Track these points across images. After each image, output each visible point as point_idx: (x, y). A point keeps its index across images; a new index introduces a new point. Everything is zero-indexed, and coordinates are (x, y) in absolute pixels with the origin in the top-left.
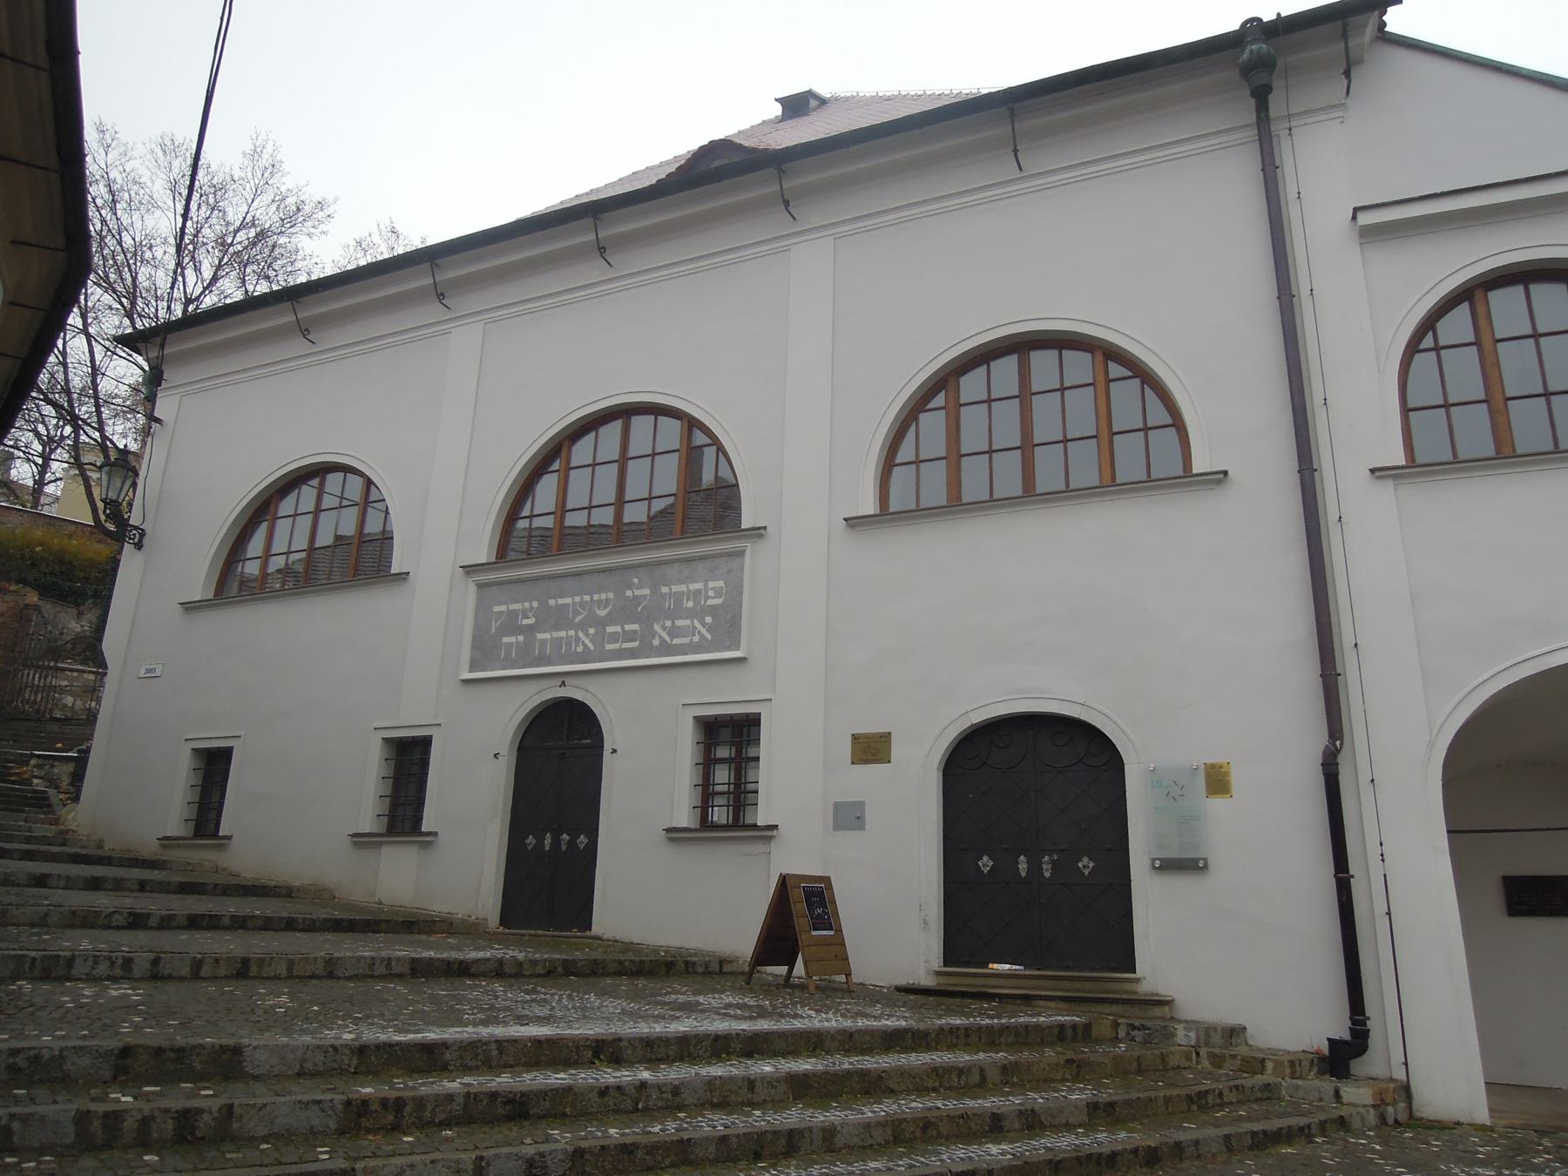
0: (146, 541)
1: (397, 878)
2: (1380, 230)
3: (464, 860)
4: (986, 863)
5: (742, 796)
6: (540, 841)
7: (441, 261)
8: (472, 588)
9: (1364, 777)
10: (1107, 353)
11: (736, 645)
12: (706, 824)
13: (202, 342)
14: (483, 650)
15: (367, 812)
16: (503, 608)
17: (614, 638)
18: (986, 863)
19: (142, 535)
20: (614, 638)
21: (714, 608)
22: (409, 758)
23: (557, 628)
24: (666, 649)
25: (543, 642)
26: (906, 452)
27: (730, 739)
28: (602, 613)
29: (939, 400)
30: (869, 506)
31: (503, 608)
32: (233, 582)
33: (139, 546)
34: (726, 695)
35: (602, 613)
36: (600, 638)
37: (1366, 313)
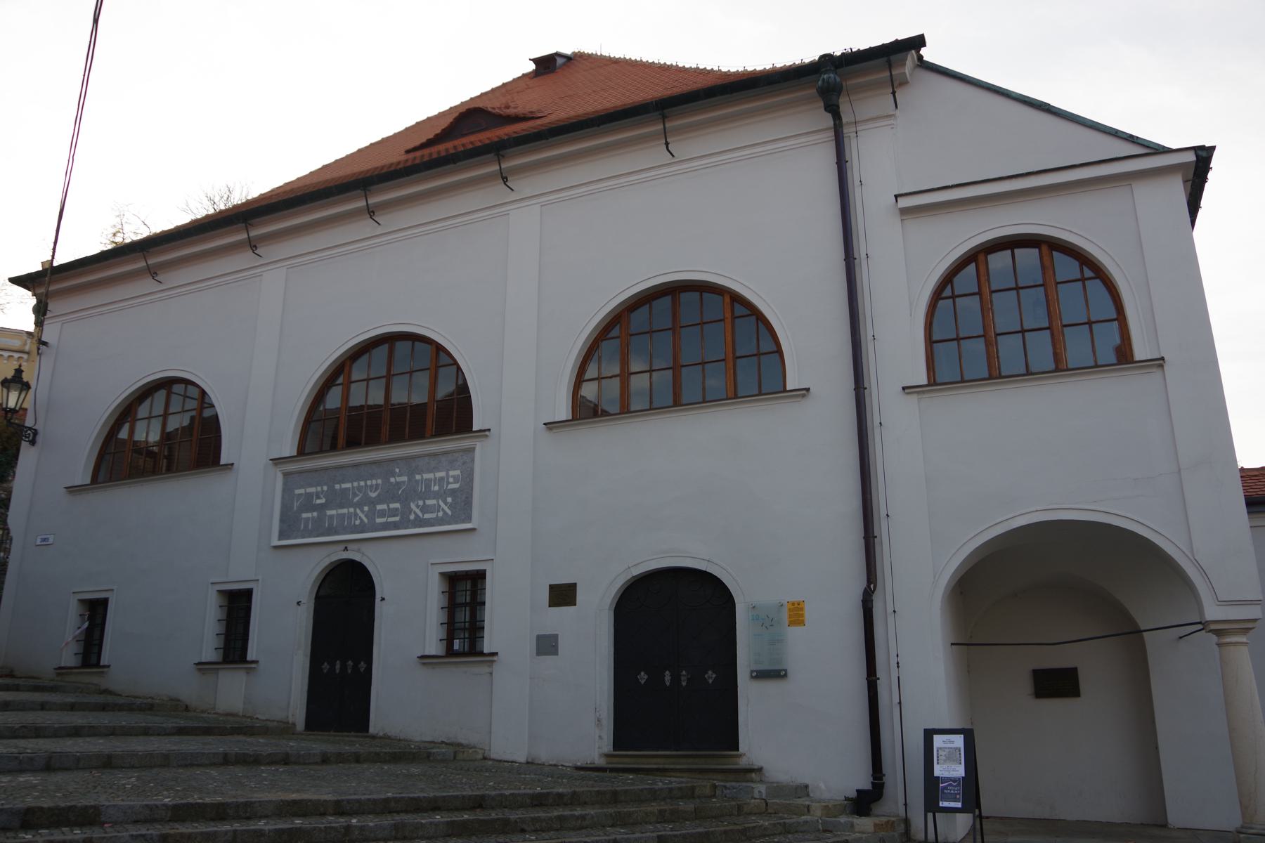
0: (39, 438)
2: (916, 209)
4: (643, 677)
5: (475, 629)
6: (333, 666)
8: (280, 478)
10: (736, 299)
11: (468, 519)
12: (450, 652)
17: (382, 514)
19: (36, 433)
20: (382, 514)
21: (453, 491)
24: (420, 522)
25: (331, 517)
27: (465, 592)
28: (373, 495)
33: (33, 442)
34: (462, 557)
35: (373, 495)
36: (372, 515)
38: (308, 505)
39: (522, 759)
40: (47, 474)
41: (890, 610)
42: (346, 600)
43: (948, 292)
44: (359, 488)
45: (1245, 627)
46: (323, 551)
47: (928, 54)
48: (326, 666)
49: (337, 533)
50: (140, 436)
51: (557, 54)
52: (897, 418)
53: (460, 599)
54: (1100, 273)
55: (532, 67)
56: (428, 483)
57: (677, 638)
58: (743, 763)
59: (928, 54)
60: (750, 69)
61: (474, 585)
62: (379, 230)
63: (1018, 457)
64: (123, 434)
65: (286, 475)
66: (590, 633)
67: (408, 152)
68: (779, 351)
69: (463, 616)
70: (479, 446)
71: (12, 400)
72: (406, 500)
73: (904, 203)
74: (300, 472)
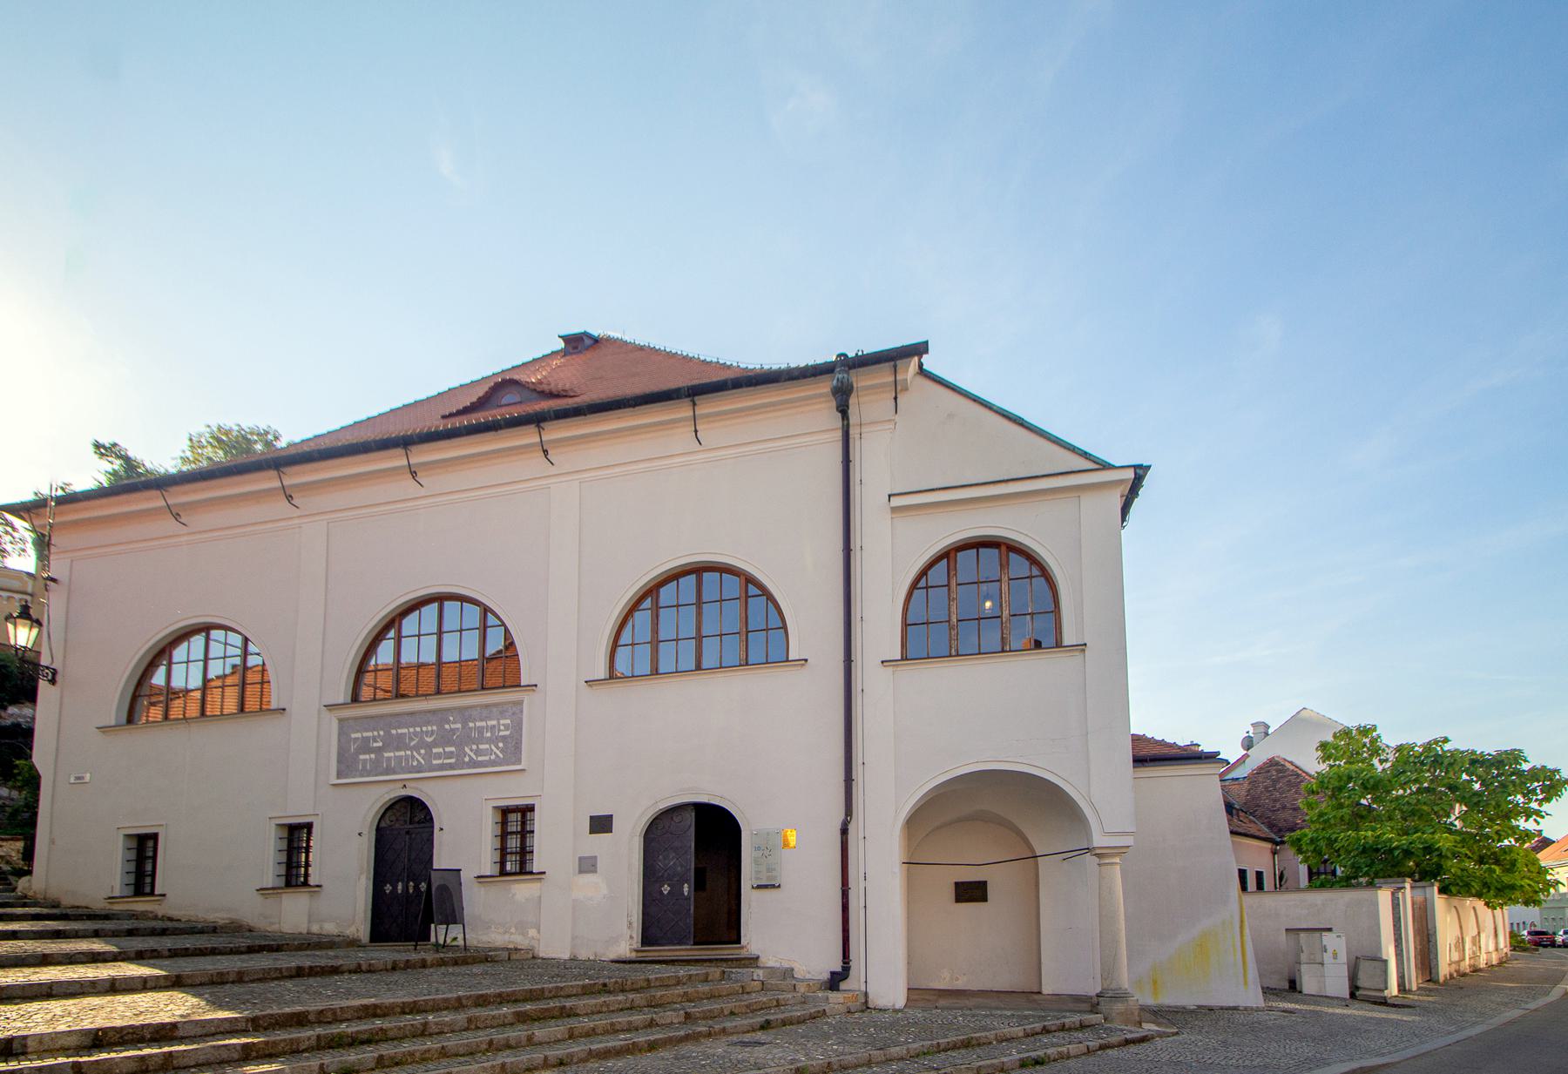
0: (59, 678)
1: (293, 914)
2: (904, 506)
3: (343, 894)
4: (666, 889)
5: (525, 853)
6: (395, 888)
7: (287, 470)
9: (861, 836)
10: (750, 580)
11: (519, 761)
12: (503, 873)
13: (869, 383)
14: (346, 765)
15: (269, 868)
16: (358, 735)
17: (438, 756)
18: (666, 889)
19: (55, 672)
20: (438, 756)
21: (504, 738)
22: (296, 837)
23: (398, 749)
25: (389, 759)
26: (626, 637)
27: (515, 825)
28: (429, 740)
29: (648, 603)
30: (601, 672)
31: (358, 735)
32: (143, 698)
33: (53, 681)
34: (513, 792)
35: (429, 740)
36: (429, 756)
37: (893, 556)
38: (365, 747)
39: (567, 957)
40: (61, 728)
41: (861, 836)
42: (404, 830)
43: (922, 583)
44: (415, 734)
45: (1120, 851)
46: (383, 789)
47: (929, 362)
48: (388, 888)
49: (395, 773)
50: (178, 682)
51: (586, 334)
52: (874, 682)
53: (512, 828)
54: (770, 598)
55: (562, 345)
56: (480, 730)
57: (700, 859)
58: (744, 953)
59: (929, 362)
60: (766, 367)
61: (524, 816)
62: (423, 492)
63: (964, 716)
64: (159, 678)
65: (341, 721)
66: (623, 855)
67: (444, 417)
68: (784, 627)
69: (513, 843)
70: (527, 698)
71: (22, 636)
72: (460, 745)
73: (896, 502)
74: (356, 719)
